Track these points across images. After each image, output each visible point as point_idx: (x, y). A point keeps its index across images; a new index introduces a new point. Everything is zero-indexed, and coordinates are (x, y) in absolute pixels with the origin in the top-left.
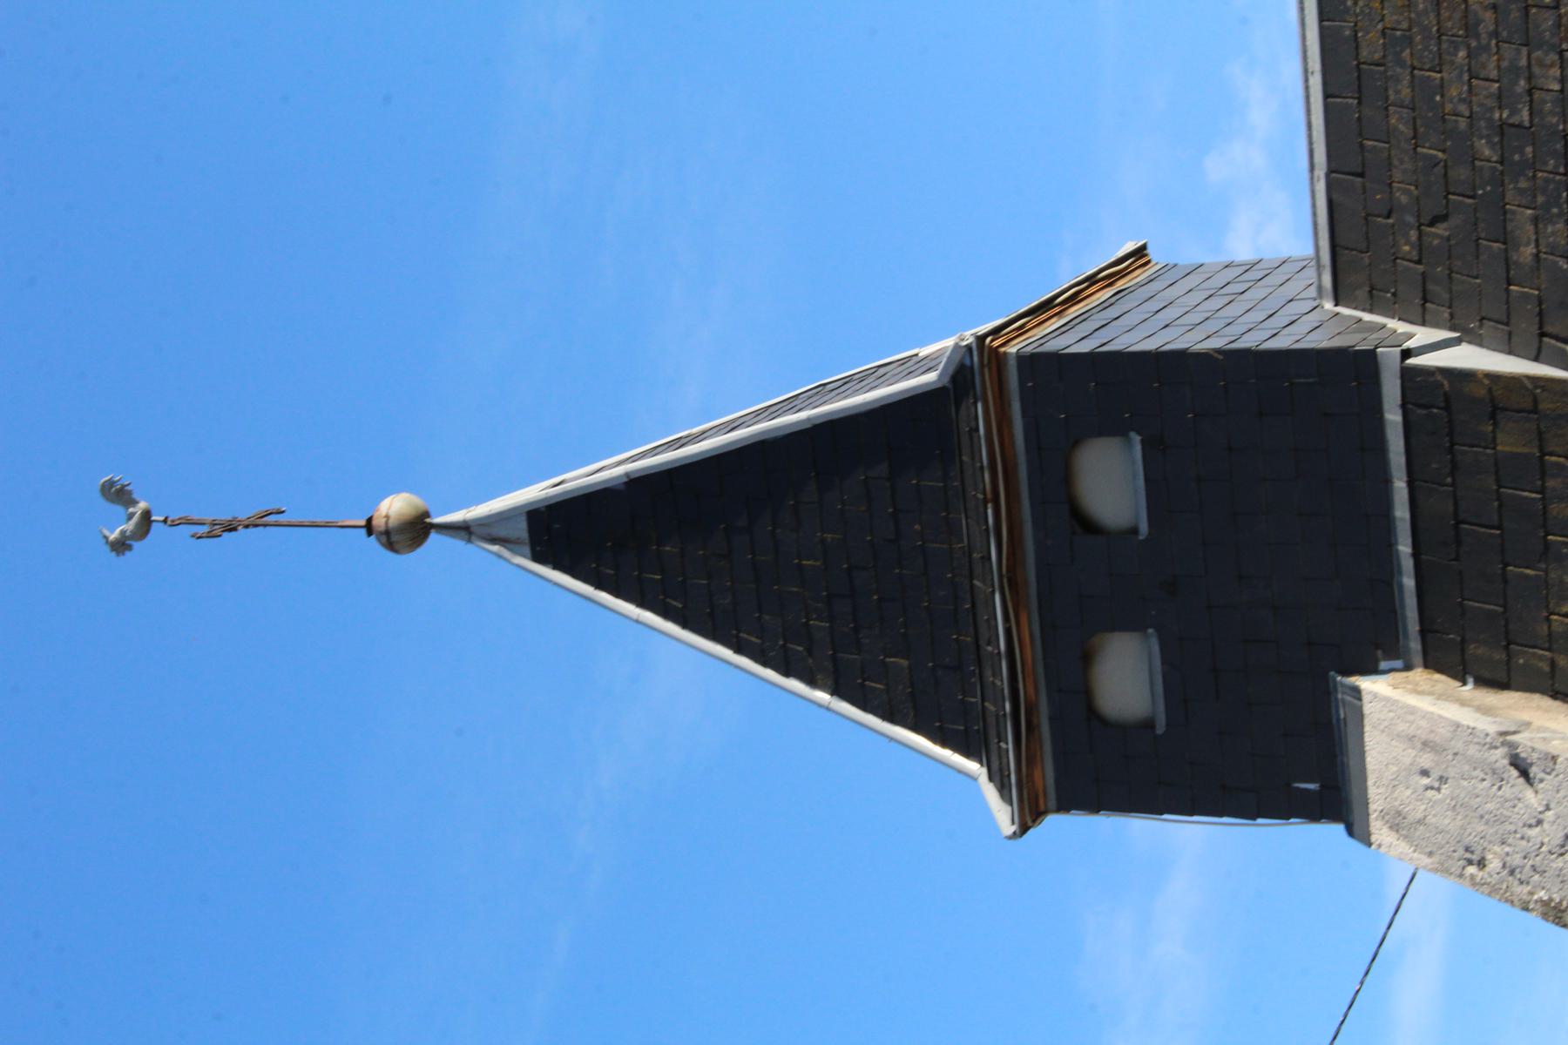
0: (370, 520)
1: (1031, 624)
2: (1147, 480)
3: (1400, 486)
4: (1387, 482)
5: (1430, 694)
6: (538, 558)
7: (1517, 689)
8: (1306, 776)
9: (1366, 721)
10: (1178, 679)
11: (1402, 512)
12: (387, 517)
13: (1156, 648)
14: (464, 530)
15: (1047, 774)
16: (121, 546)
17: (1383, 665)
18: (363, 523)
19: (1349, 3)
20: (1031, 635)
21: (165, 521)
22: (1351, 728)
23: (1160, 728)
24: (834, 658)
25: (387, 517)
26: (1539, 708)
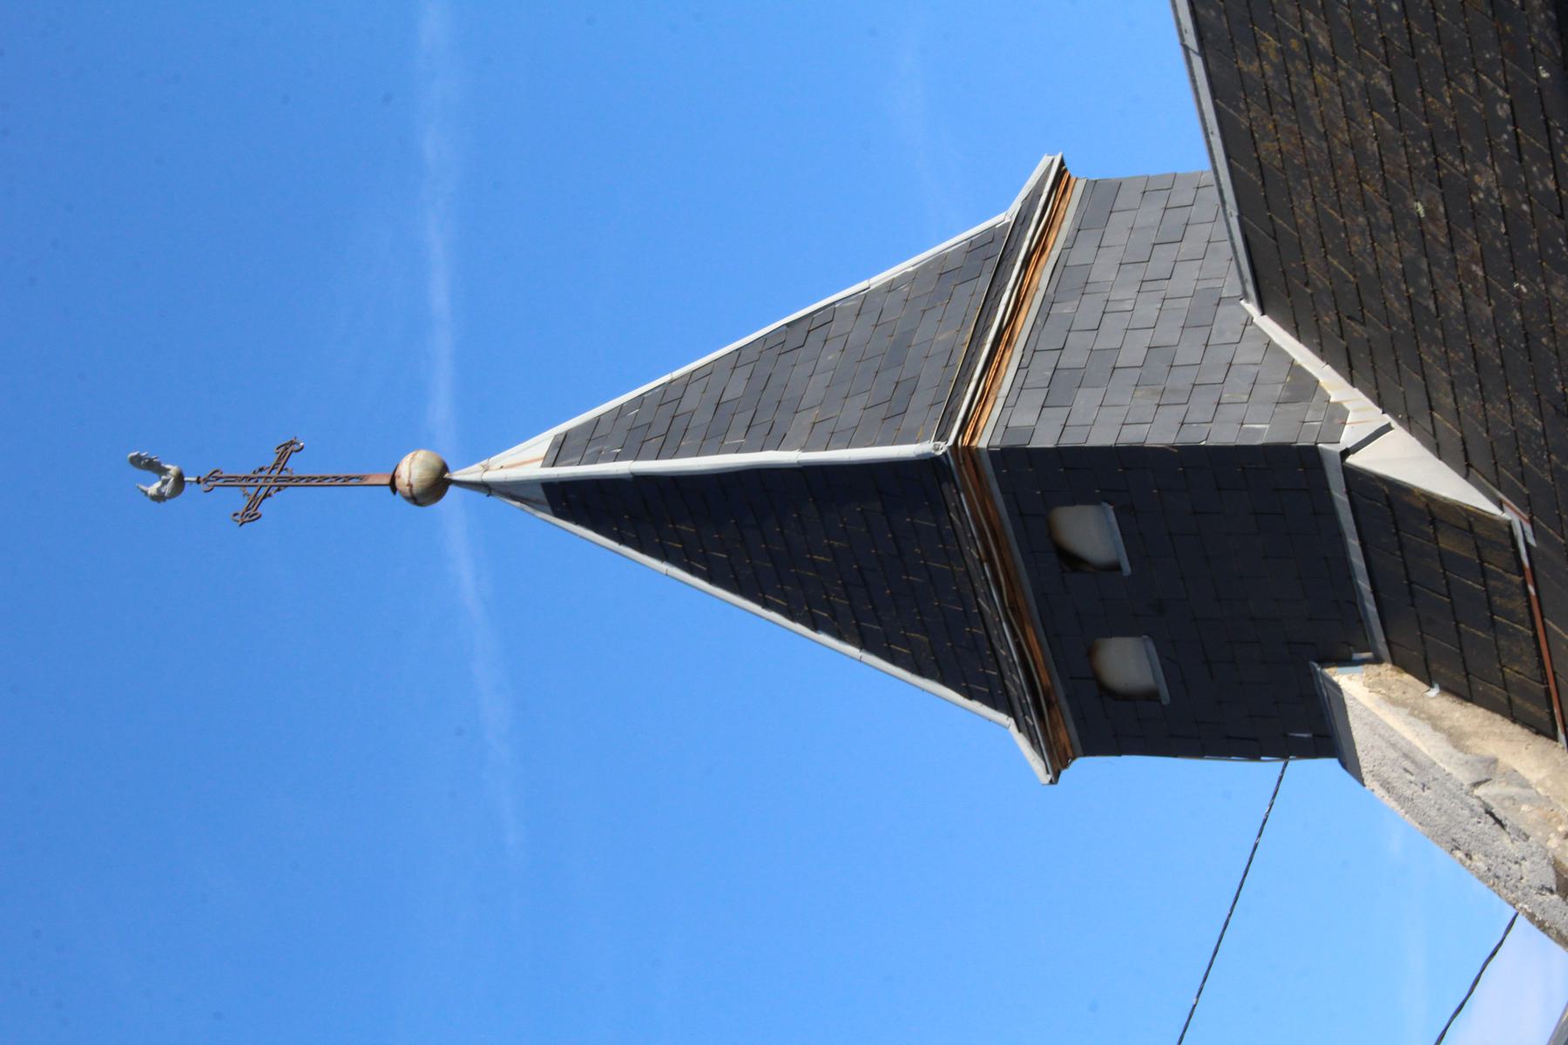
0: (393, 479)
2: (1122, 535)
3: (1353, 543)
5: (1404, 705)
6: (557, 515)
7: (1480, 705)
9: (1350, 714)
11: (1358, 561)
12: (410, 485)
13: (1152, 649)
14: (486, 487)
15: (1067, 734)
17: (1356, 656)
18: (387, 480)
20: (1039, 642)
21: (198, 482)
22: (1333, 703)
23: (1165, 697)
24: (858, 626)
25: (410, 485)
26: (1502, 734)
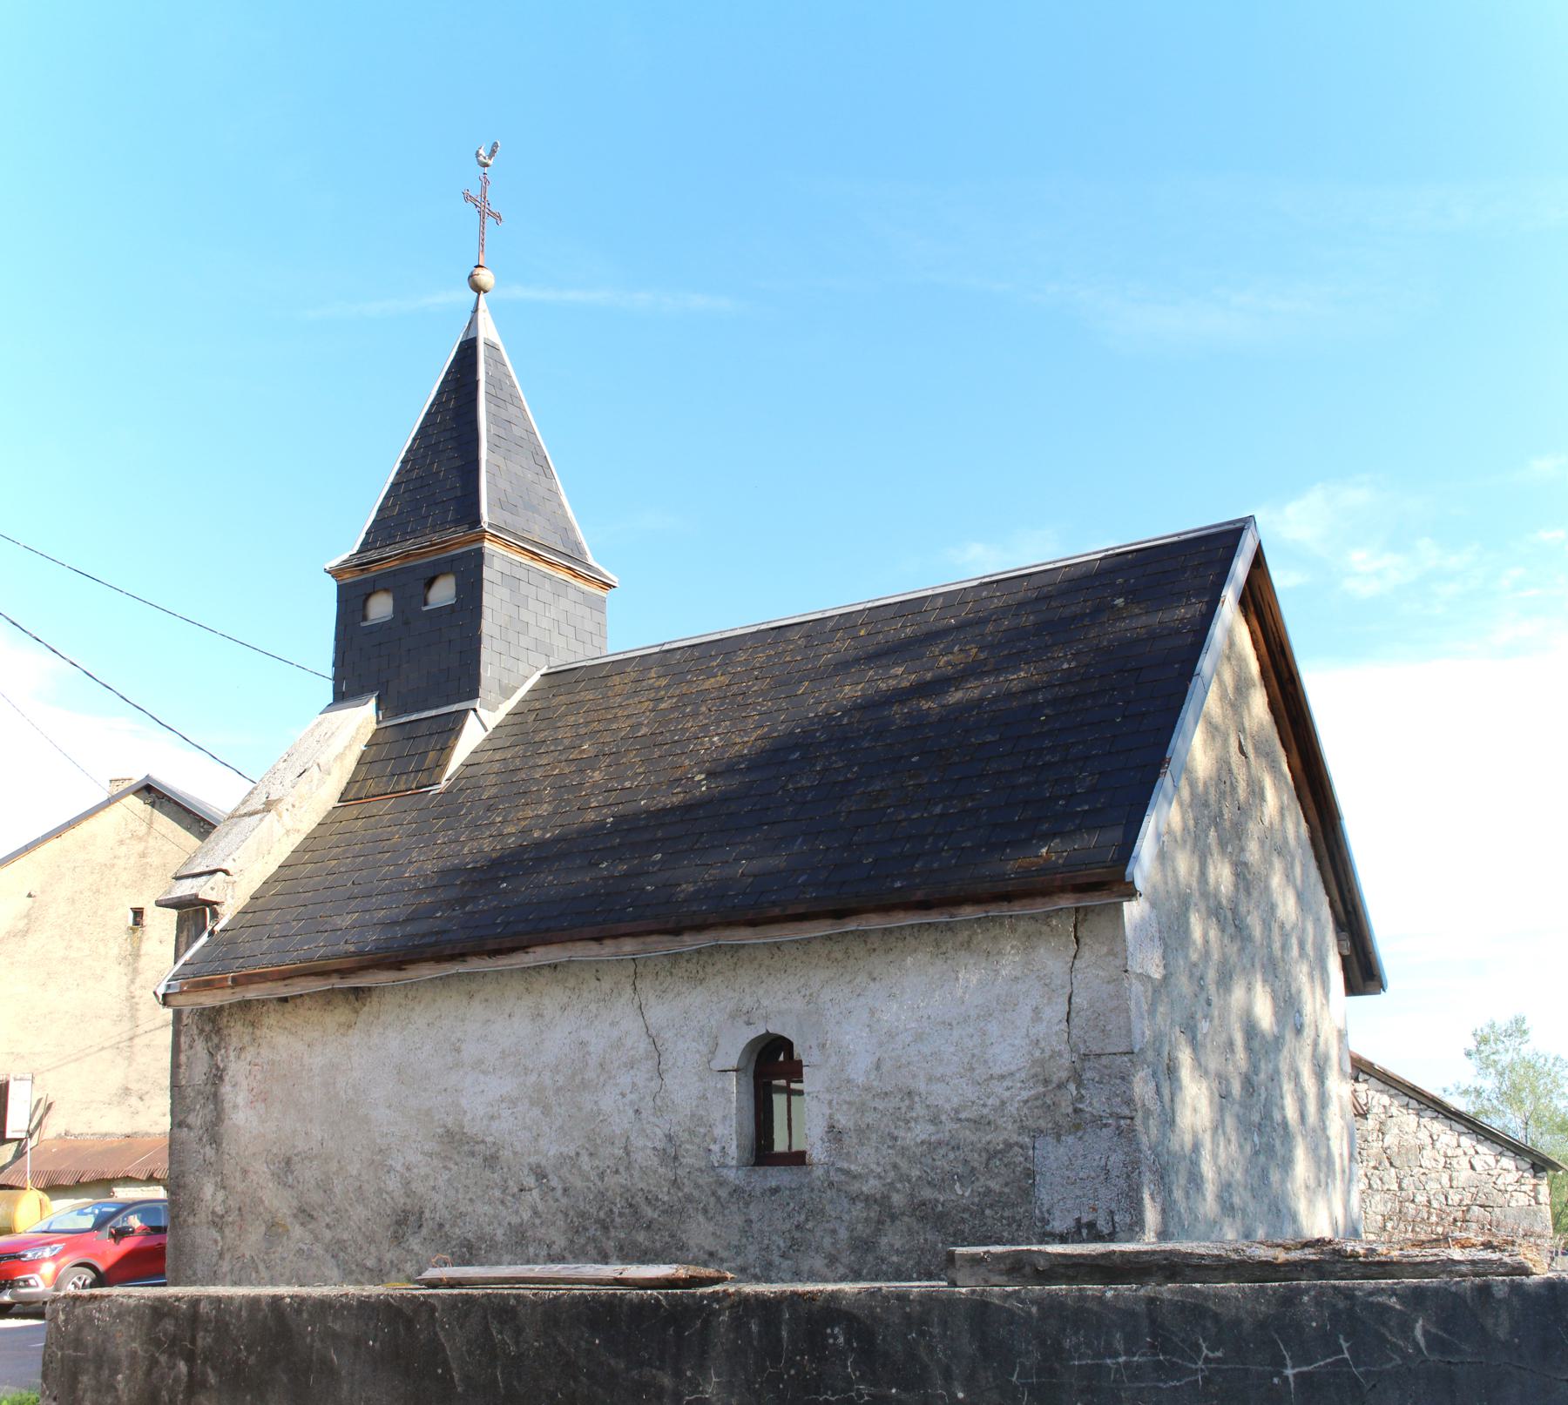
1: (394, 564)
3: (433, 713)
4: (437, 707)
8: (345, 692)
10: (381, 627)
16: (478, 155)
19: (734, 1401)
